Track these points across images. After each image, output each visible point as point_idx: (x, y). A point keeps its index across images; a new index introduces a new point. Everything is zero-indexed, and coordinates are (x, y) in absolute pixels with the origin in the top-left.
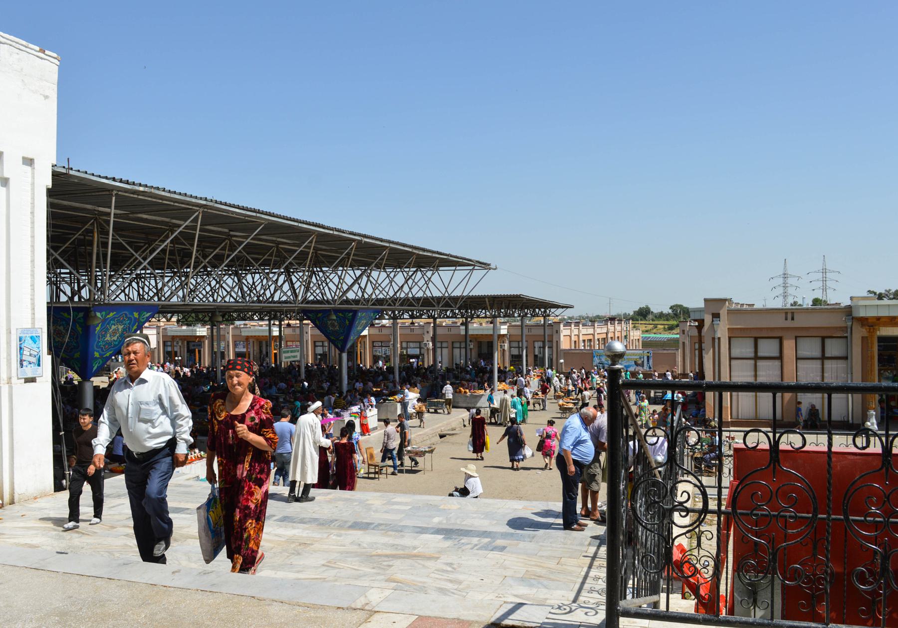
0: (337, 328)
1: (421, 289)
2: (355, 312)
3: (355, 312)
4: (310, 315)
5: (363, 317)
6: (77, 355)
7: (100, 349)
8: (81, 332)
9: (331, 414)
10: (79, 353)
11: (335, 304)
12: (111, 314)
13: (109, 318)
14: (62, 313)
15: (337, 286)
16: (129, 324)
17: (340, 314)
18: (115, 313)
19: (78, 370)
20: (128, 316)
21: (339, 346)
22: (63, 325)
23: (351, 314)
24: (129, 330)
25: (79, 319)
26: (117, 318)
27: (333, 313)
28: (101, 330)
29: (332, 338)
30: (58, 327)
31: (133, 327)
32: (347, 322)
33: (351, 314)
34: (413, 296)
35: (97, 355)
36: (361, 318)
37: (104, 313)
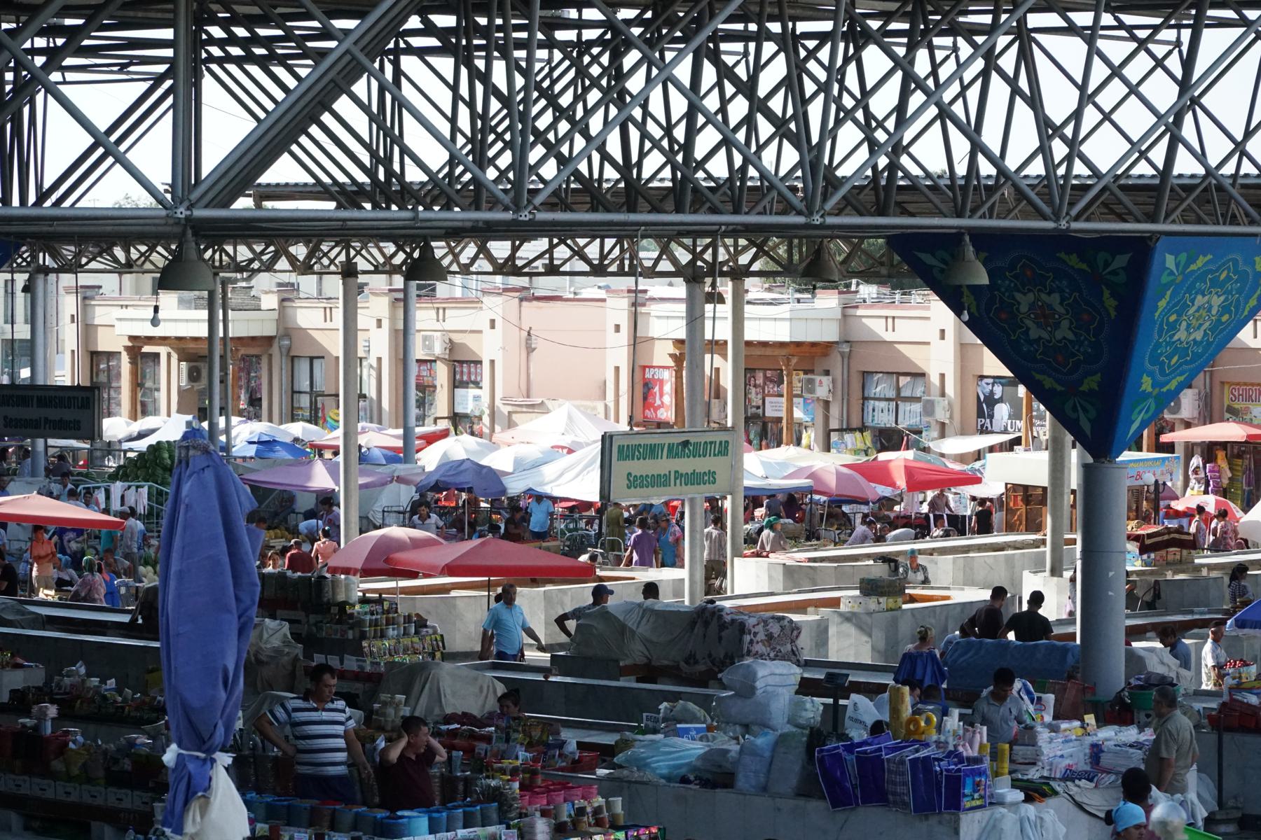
0: (1064, 331)
1: (1107, 117)
2: (1141, 248)
3: (1141, 248)
4: (927, 258)
5: (1202, 277)
6: (1091, 383)
7: (1156, 368)
8: (1113, 314)
9: (1012, 728)
10: (1098, 377)
11: (1057, 217)
12: (1201, 261)
13: (1193, 271)
14: (1062, 255)
15: (454, 88)
16: (1240, 291)
17: (1073, 260)
18: (1209, 257)
19: (1086, 427)
20: (1241, 267)
21: (1086, 427)
22: (1061, 291)
23: (1121, 261)
24: (1237, 308)
25: (1114, 273)
26: (1211, 272)
27: (970, 251)
28: (1168, 311)
29: (1048, 383)
30: (1044, 296)
31: (1247, 302)
32: (1110, 303)
33: (1121, 261)
34: (1209, 172)
35: (1147, 384)
36: (1189, 285)
37: (1183, 257)
